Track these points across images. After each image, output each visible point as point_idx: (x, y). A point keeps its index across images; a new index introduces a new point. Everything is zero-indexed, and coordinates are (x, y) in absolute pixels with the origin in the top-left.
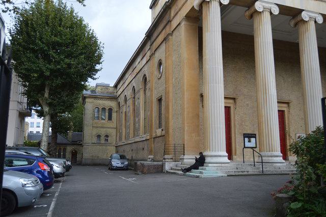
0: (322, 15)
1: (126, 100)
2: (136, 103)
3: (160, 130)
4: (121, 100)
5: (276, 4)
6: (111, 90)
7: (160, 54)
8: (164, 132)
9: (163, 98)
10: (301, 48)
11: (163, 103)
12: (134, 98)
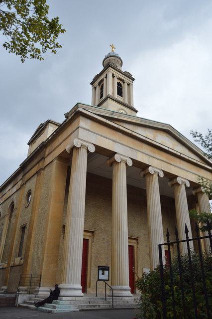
0: (164, 171)
3: (19, 258)
7: (31, 185)
9: (27, 226)
11: (26, 231)
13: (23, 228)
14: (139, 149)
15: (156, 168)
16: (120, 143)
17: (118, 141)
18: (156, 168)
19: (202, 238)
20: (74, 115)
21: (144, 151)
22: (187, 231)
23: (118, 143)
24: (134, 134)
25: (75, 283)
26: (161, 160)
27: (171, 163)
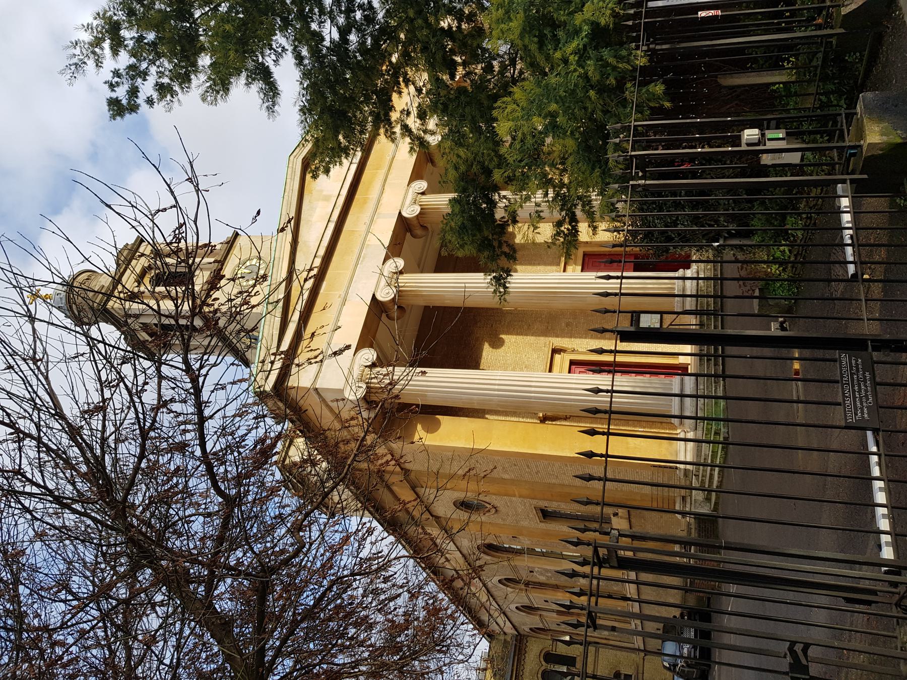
0: (412, 180)
1: (529, 609)
2: (542, 579)
3: (614, 520)
4: (527, 622)
5: (354, 355)
6: (498, 648)
7: (444, 506)
8: (621, 511)
9: (543, 504)
10: (438, 304)
11: (553, 506)
12: (527, 584)
13: (546, 515)
14: (361, 239)
15: (405, 198)
16: (348, 288)
17: (342, 293)
18: (405, 198)
19: (610, 416)
20: (281, 400)
21: (364, 228)
22: (601, 351)
23: (347, 293)
24: (322, 252)
25: (736, 456)
26: (384, 186)
27: (389, 158)
